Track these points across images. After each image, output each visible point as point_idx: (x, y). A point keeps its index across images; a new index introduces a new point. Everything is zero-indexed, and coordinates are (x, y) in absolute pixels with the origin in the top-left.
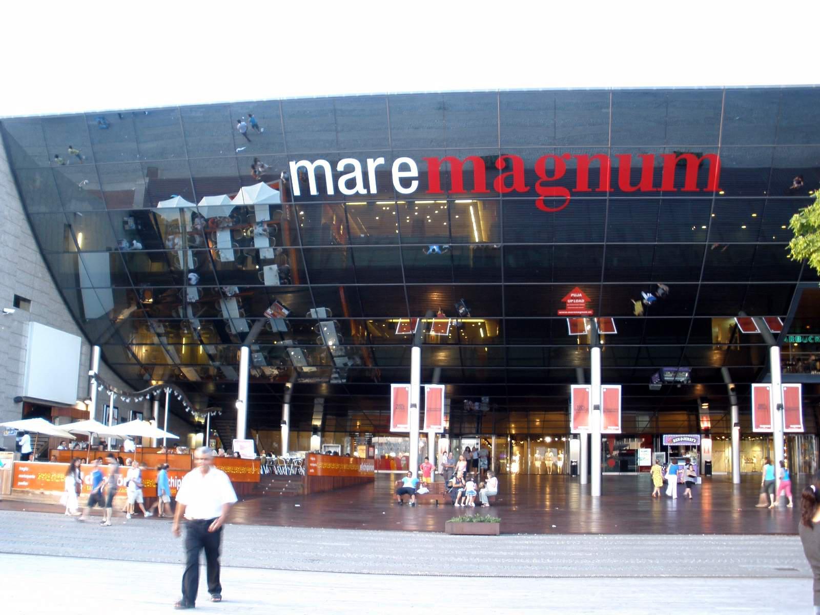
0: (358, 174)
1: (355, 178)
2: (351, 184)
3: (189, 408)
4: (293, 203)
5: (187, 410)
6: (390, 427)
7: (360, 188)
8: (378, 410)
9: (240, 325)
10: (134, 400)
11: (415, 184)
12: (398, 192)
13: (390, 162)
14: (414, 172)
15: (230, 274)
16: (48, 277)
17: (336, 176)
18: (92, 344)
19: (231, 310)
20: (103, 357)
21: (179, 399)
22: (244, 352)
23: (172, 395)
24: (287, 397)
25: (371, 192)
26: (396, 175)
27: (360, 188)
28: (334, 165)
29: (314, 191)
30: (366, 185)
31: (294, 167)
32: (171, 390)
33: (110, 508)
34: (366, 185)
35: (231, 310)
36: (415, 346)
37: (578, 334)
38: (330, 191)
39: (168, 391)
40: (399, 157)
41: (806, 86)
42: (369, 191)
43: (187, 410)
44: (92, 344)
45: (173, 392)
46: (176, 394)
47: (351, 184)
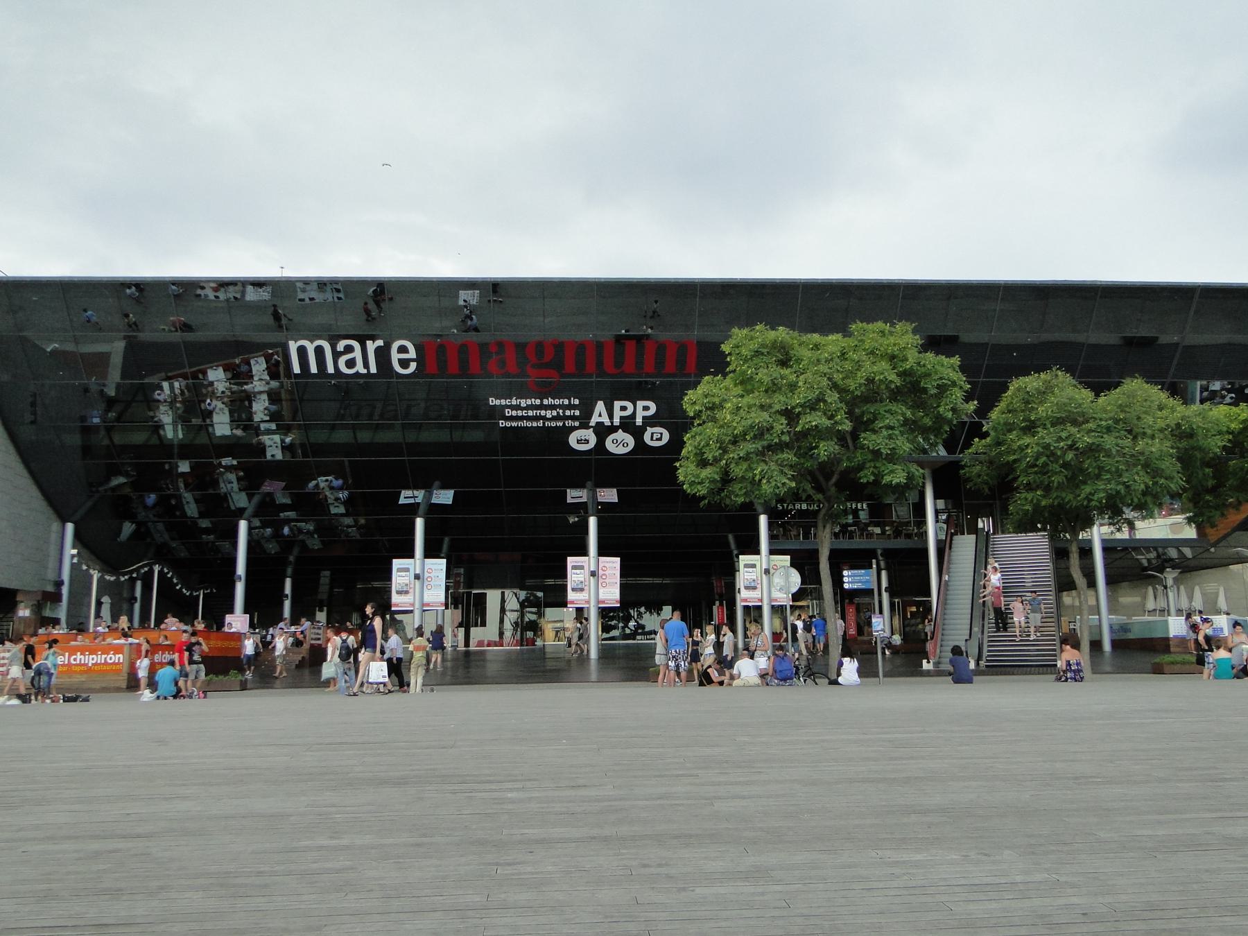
0: (357, 353)
1: (355, 358)
2: (351, 363)
3: (180, 586)
4: (293, 380)
5: (178, 588)
6: (567, 590)
7: (360, 368)
8: (464, 579)
9: (240, 500)
10: (119, 579)
11: (413, 366)
12: (398, 373)
13: (387, 346)
14: (412, 354)
15: (228, 447)
16: (12, 449)
17: (336, 355)
18: (64, 520)
19: (230, 484)
20: (78, 536)
21: (169, 576)
22: (243, 526)
23: (160, 572)
24: (289, 571)
25: (372, 372)
26: (395, 357)
27: (360, 368)
28: (333, 347)
29: (314, 369)
30: (366, 365)
31: (293, 346)
32: (160, 567)
33: (125, 687)
34: (366, 365)
35: (230, 484)
36: (419, 517)
37: (981, 502)
38: (331, 370)
39: (157, 568)
40: (394, 341)
41: (666, 280)
42: (368, 371)
43: (178, 588)
44: (64, 520)
45: (162, 569)
46: (166, 570)
47: (351, 363)
